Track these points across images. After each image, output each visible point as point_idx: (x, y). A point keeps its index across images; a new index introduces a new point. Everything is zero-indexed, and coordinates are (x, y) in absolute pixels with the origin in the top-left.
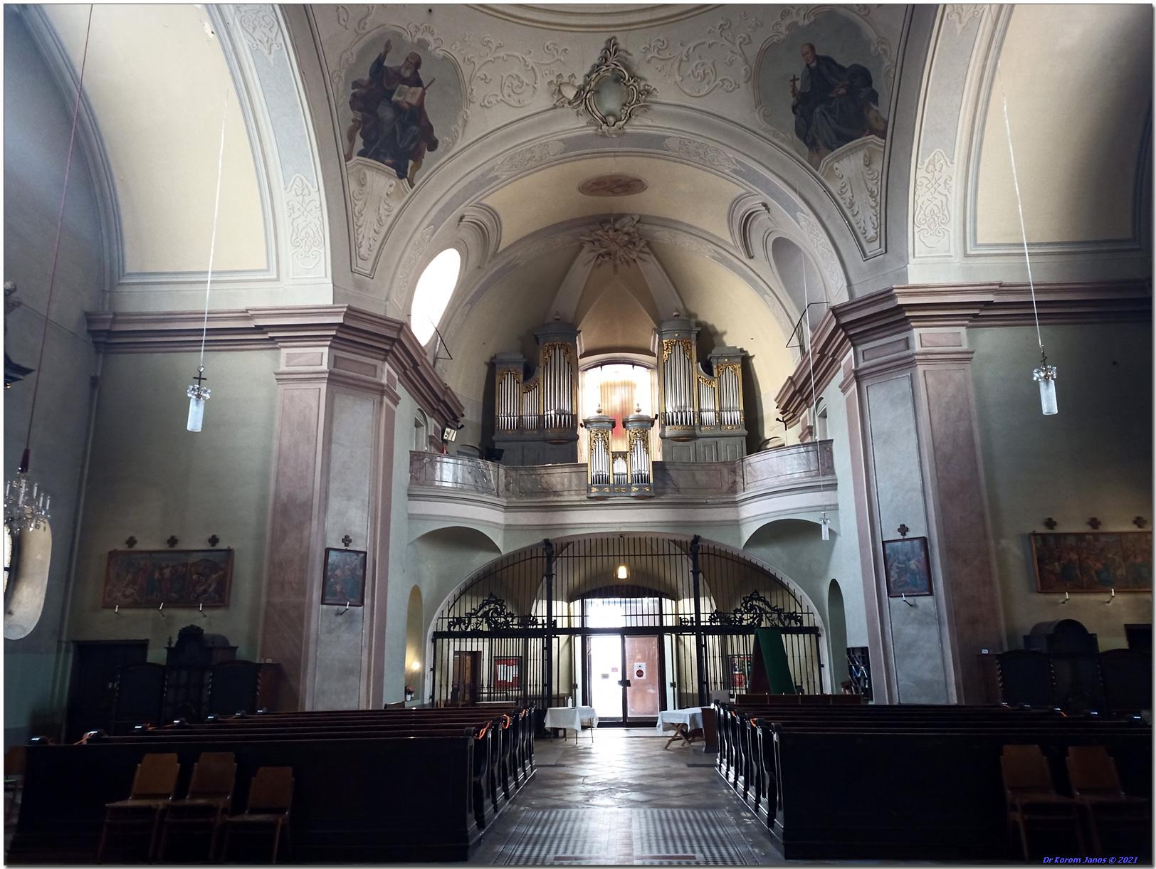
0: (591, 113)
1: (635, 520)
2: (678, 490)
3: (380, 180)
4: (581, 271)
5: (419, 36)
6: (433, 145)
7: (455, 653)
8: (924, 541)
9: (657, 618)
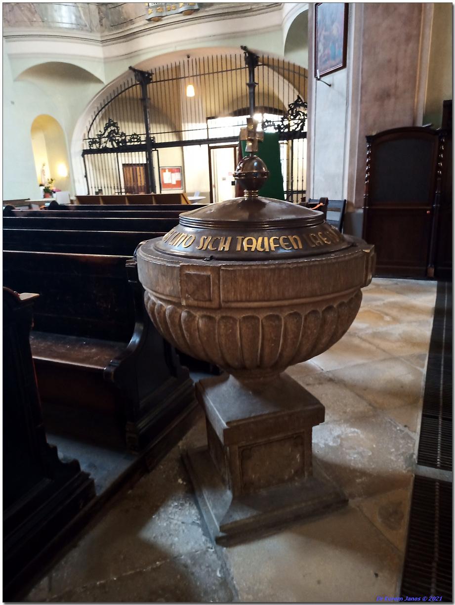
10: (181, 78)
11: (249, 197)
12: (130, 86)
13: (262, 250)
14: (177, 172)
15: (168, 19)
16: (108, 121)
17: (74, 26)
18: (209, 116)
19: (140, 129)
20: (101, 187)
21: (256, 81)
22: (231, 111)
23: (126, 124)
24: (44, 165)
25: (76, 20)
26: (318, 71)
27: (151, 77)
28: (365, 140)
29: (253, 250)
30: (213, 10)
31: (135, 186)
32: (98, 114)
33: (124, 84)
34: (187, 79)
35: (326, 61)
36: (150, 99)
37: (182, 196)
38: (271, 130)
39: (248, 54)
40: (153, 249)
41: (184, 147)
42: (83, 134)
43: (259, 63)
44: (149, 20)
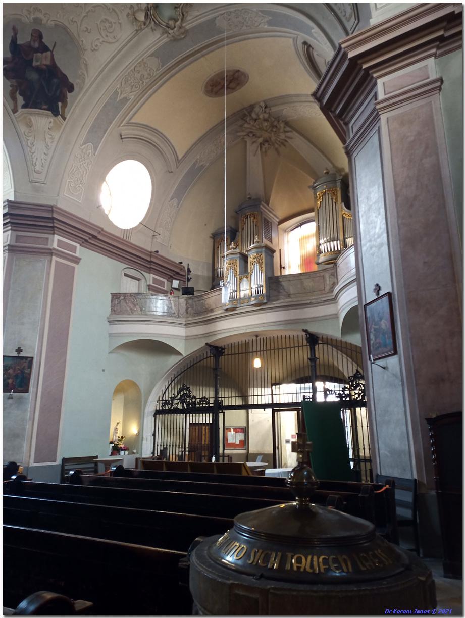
0: (158, 24)
1: (257, 322)
2: (289, 296)
3: (42, 120)
4: (255, 161)
5: (32, 16)
6: (71, 88)
7: (190, 424)
8: (389, 295)
9: (274, 393)
10: (250, 352)
11: (301, 504)
12: (205, 358)
13: (311, 571)
15: (243, 309)
16: (182, 385)
17: (165, 314)
18: (273, 383)
19: (209, 394)
20: (167, 446)
21: (317, 356)
22: (294, 378)
23: (198, 388)
24: (118, 424)
25: (167, 309)
26: (371, 356)
27: (223, 351)
28: (425, 422)
29: (302, 570)
31: (199, 445)
32: (174, 380)
33: (200, 356)
34: (255, 354)
35: (378, 347)
36: (221, 368)
37: (243, 467)
38: (332, 398)
40: (206, 554)
41: (250, 410)
42: (158, 397)
43: (320, 342)
44: (226, 310)
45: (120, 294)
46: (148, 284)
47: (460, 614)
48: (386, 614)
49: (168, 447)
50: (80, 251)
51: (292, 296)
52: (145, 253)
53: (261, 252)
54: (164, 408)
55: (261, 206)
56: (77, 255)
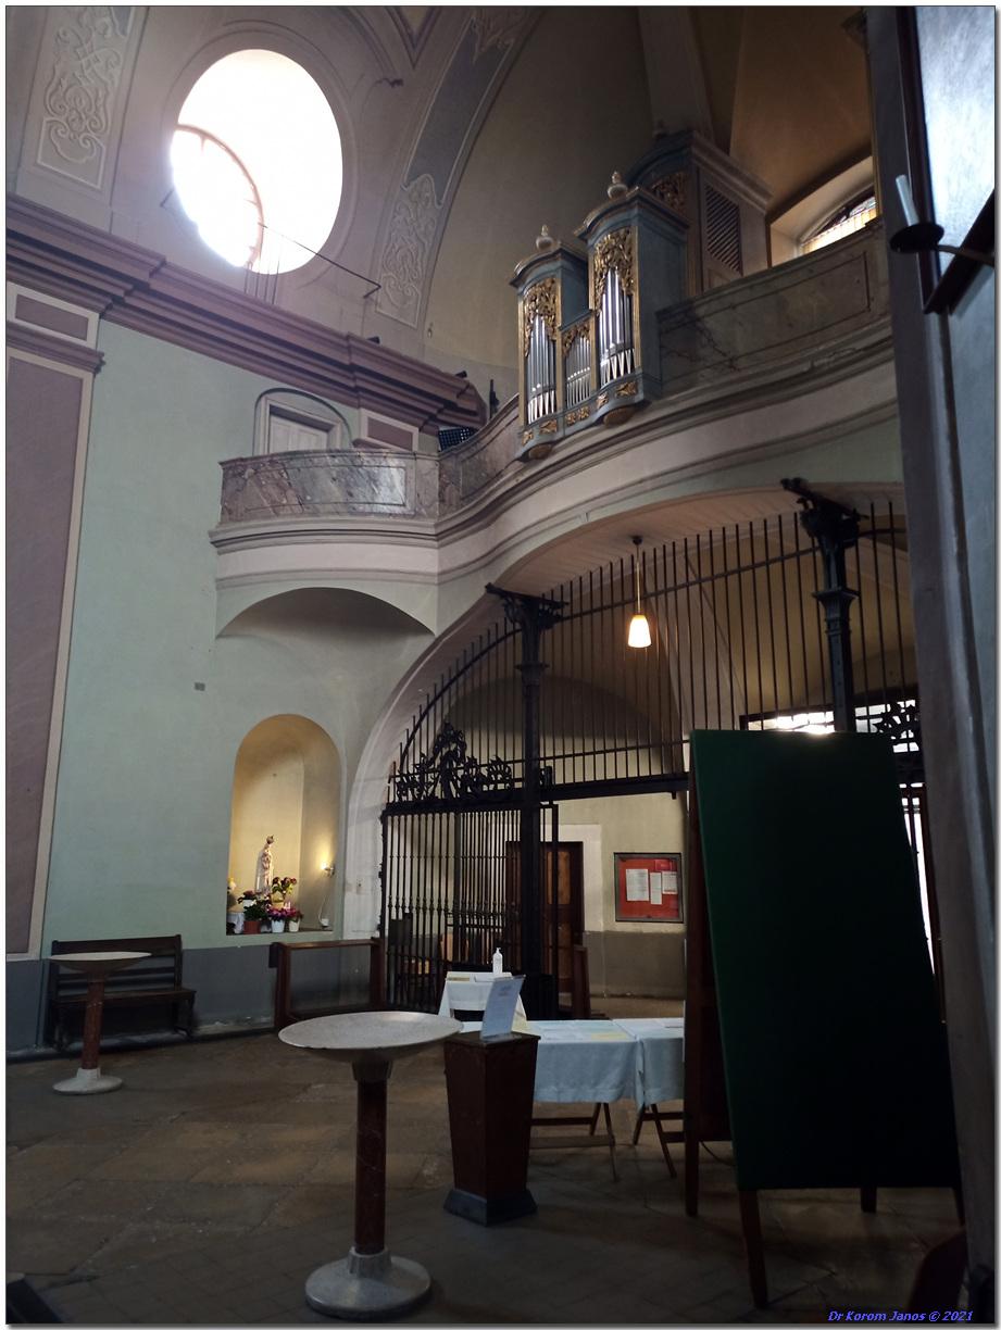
2: (731, 364)
14: (668, 869)
21: (852, 584)
24: (269, 842)
30: (695, 395)
39: (814, 504)
44: (525, 458)
45: (242, 460)
46: (355, 437)
47: (991, 1321)
48: (831, 1322)
49: (414, 911)
50: (98, 333)
51: (742, 363)
52: (331, 342)
53: (627, 225)
54: (404, 798)
55: (695, 151)
56: (90, 343)
